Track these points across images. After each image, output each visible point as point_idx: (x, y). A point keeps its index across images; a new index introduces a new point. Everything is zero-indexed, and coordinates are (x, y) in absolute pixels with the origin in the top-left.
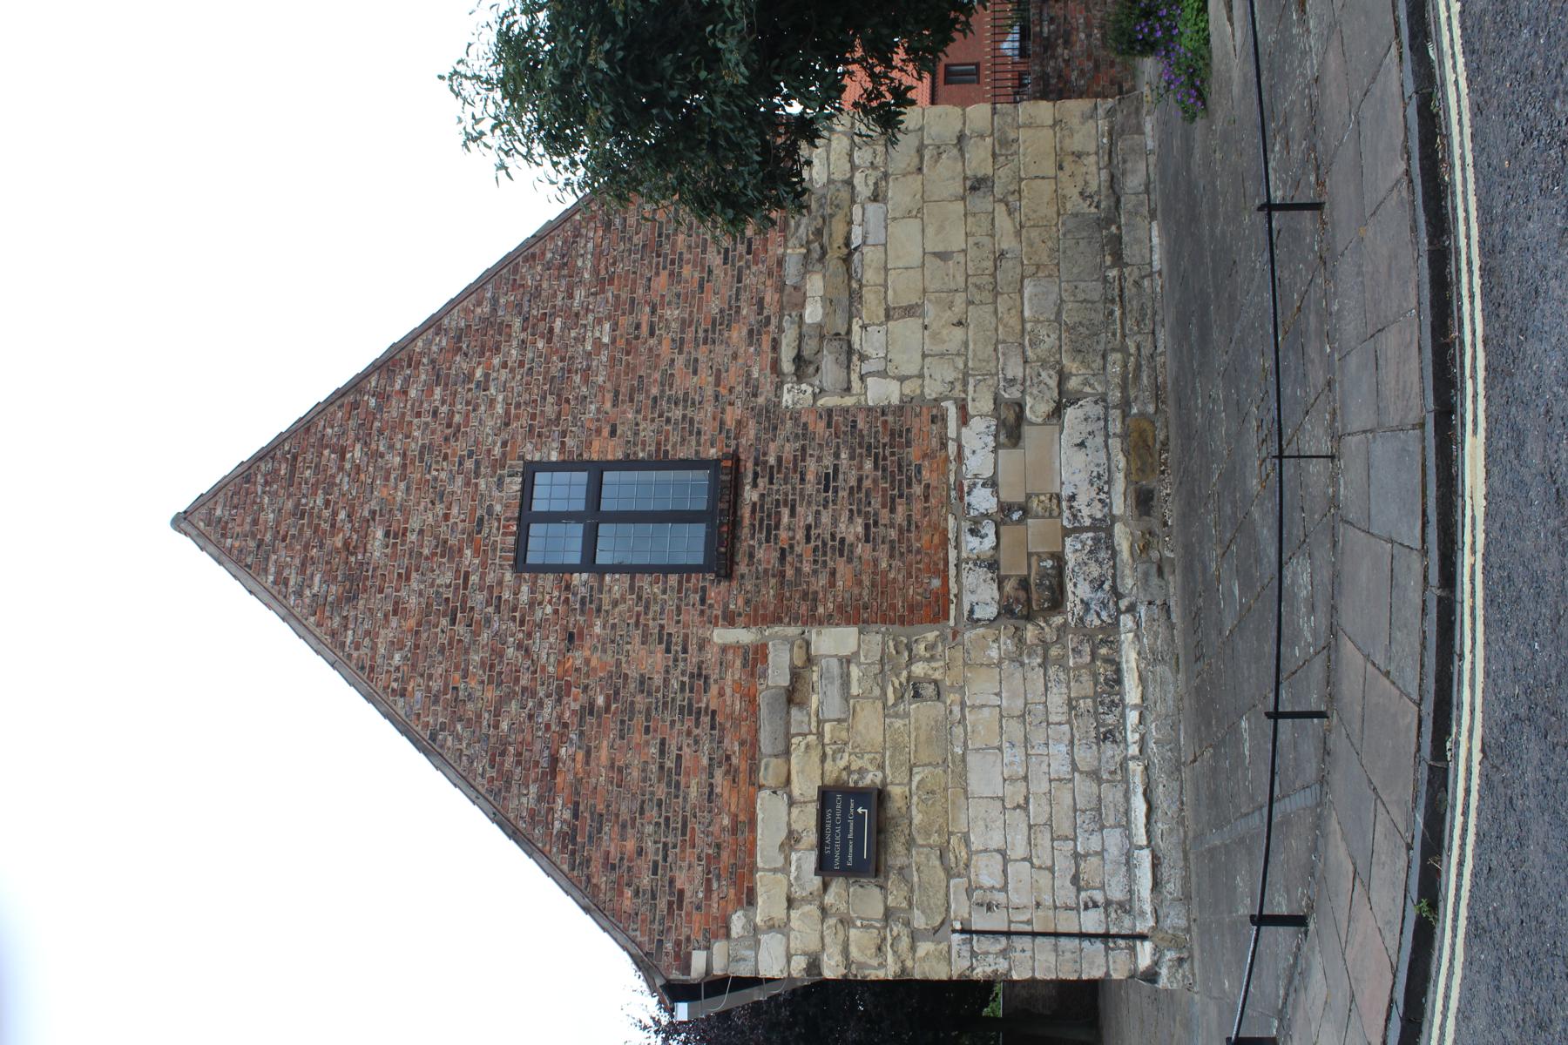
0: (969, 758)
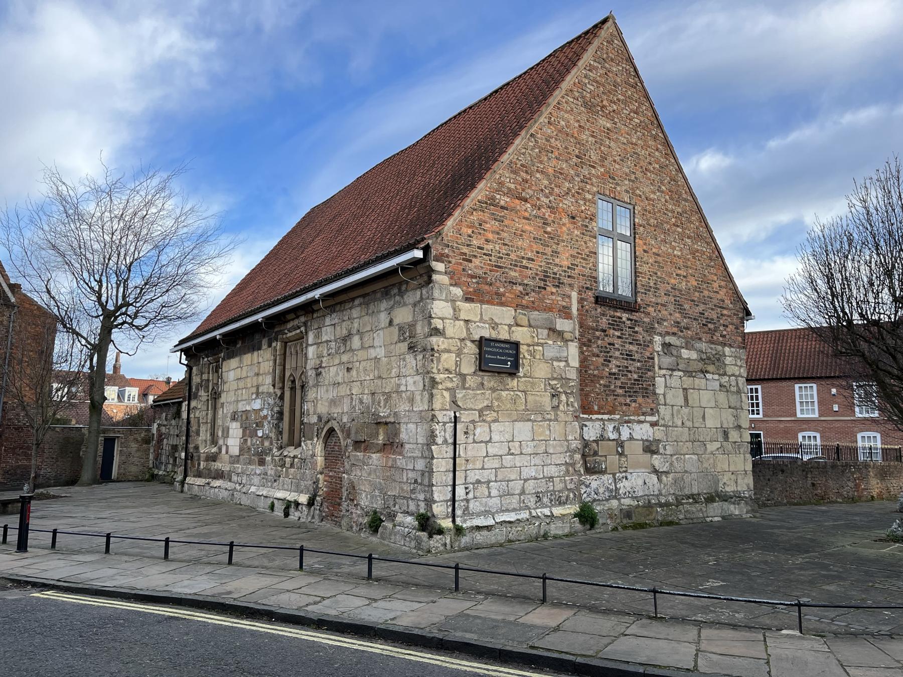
0: (530, 423)
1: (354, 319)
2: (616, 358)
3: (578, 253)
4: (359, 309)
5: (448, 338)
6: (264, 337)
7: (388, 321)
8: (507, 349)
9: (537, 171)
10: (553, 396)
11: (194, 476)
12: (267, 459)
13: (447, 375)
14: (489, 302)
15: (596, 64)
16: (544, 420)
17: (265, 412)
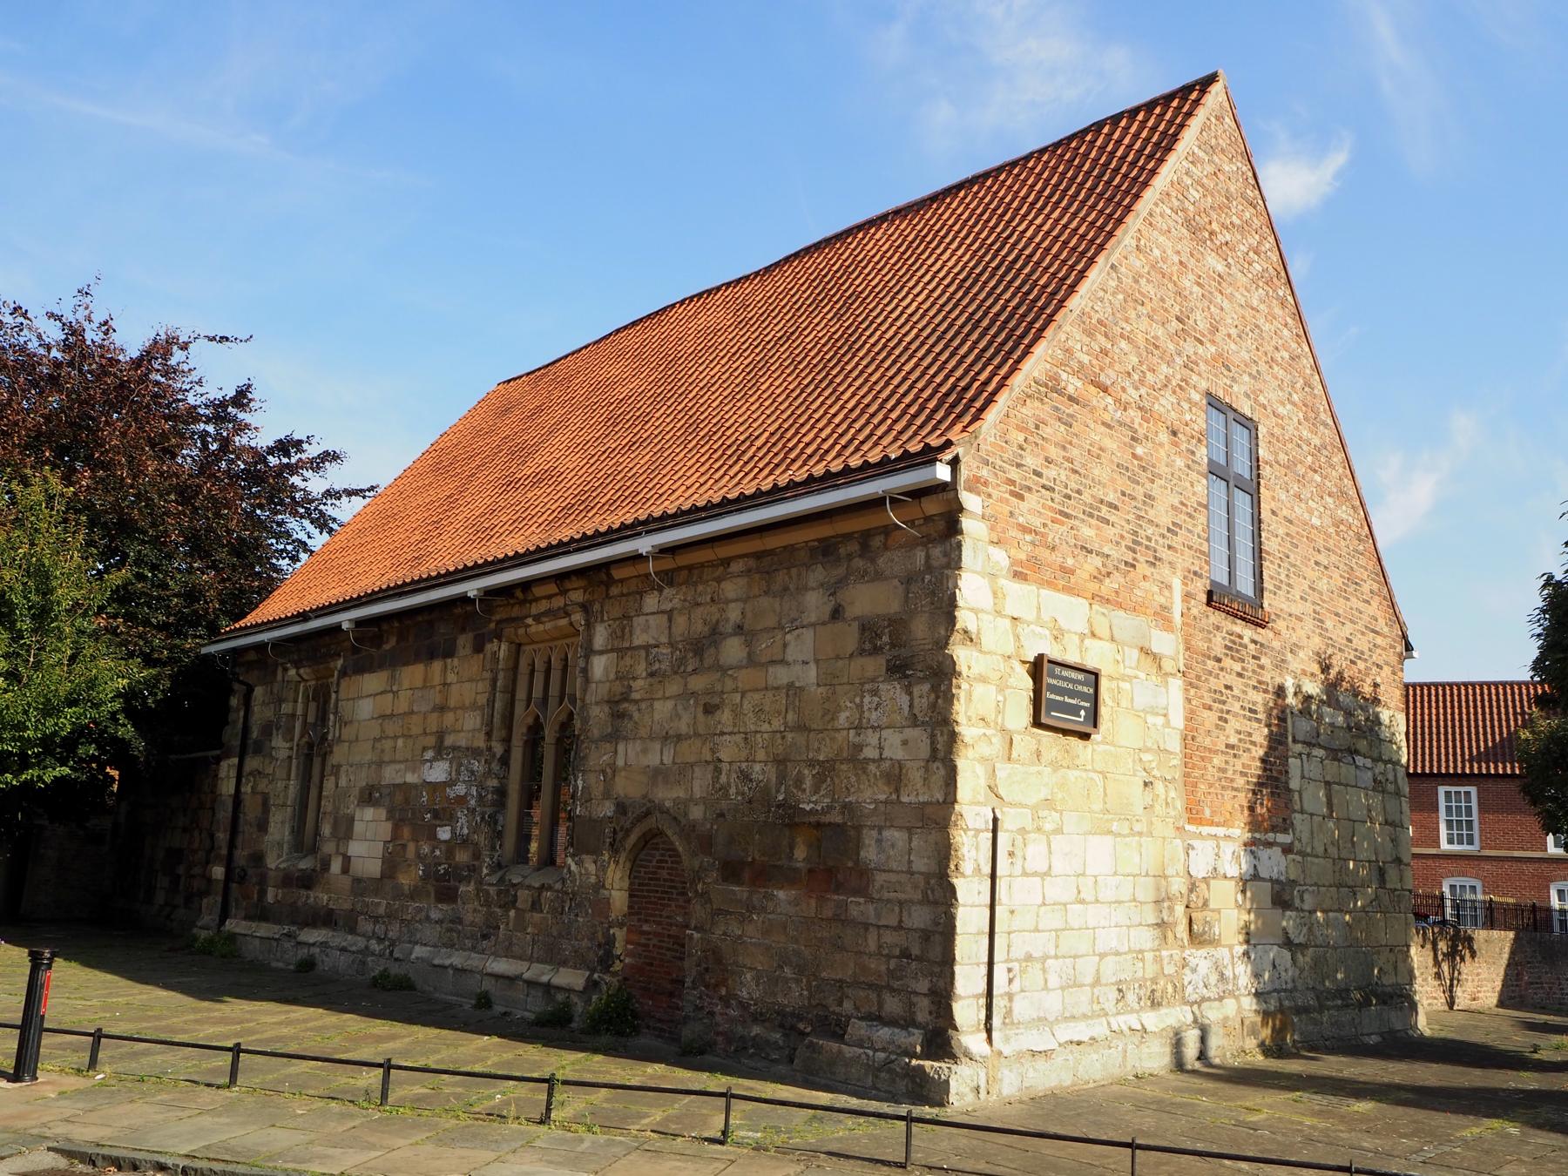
0: (1110, 838)
1: (728, 602)
2: (1236, 715)
3: (1182, 503)
4: (742, 581)
5: (985, 653)
6: (463, 630)
7: (828, 609)
8: (1079, 682)
9: (1122, 336)
10: (1146, 784)
11: (248, 918)
12: (462, 888)
13: (983, 731)
14: (1050, 584)
15: (1201, 154)
16: (1133, 833)
17: (460, 789)
